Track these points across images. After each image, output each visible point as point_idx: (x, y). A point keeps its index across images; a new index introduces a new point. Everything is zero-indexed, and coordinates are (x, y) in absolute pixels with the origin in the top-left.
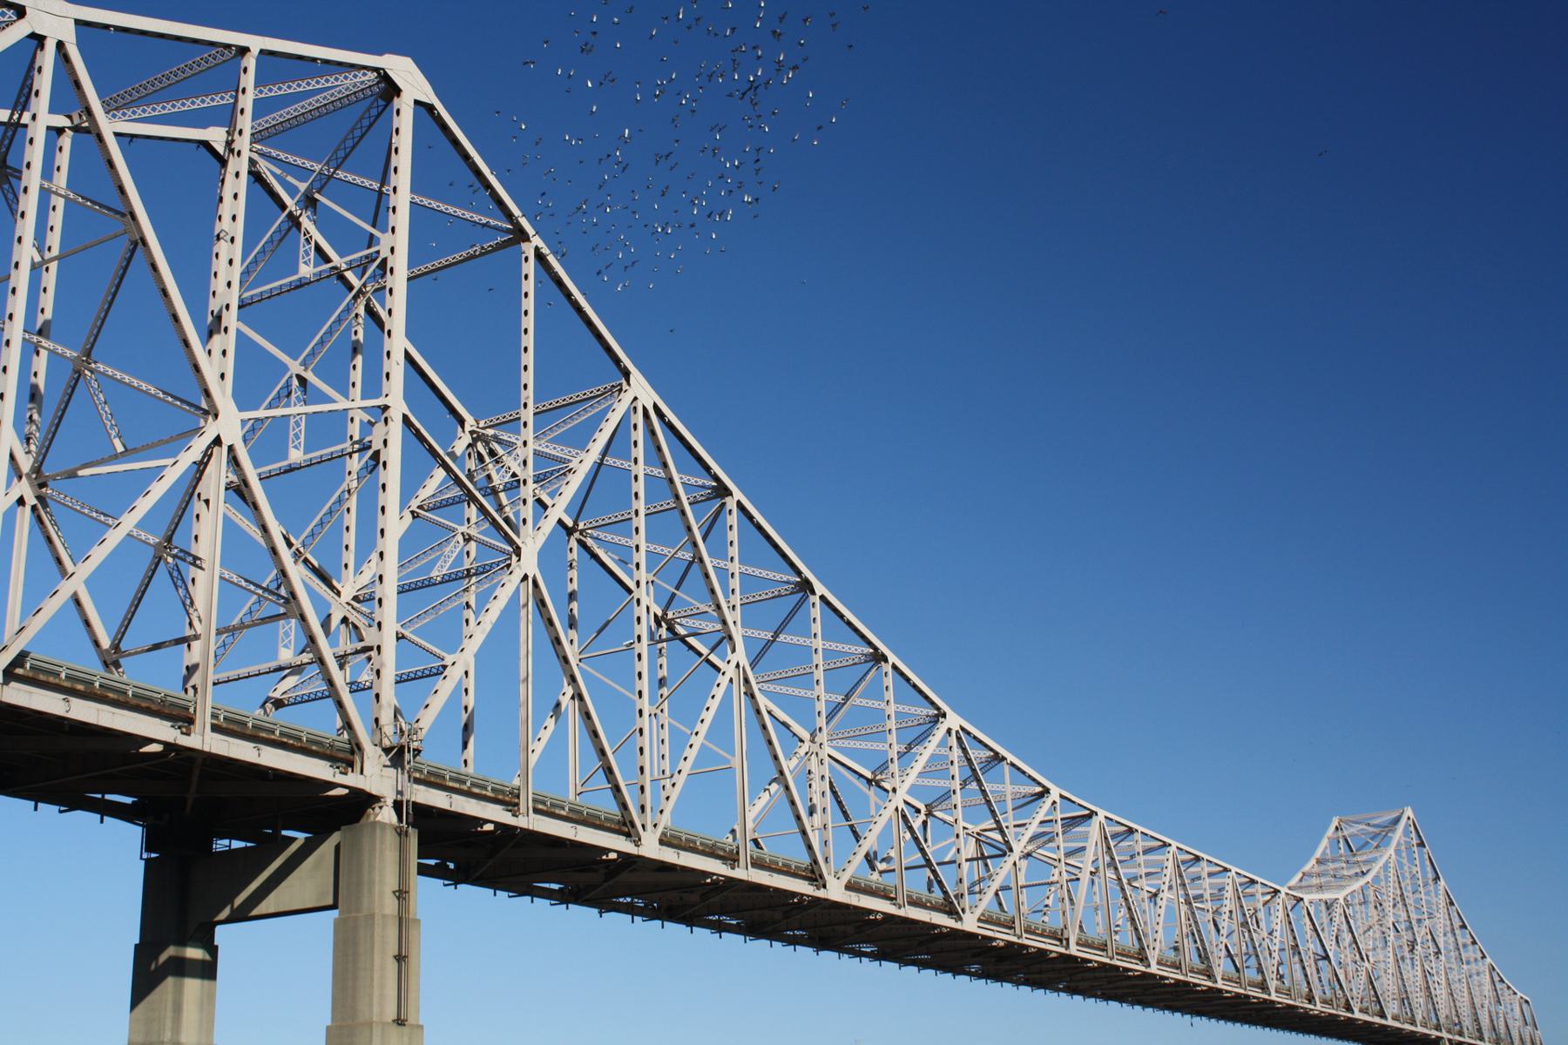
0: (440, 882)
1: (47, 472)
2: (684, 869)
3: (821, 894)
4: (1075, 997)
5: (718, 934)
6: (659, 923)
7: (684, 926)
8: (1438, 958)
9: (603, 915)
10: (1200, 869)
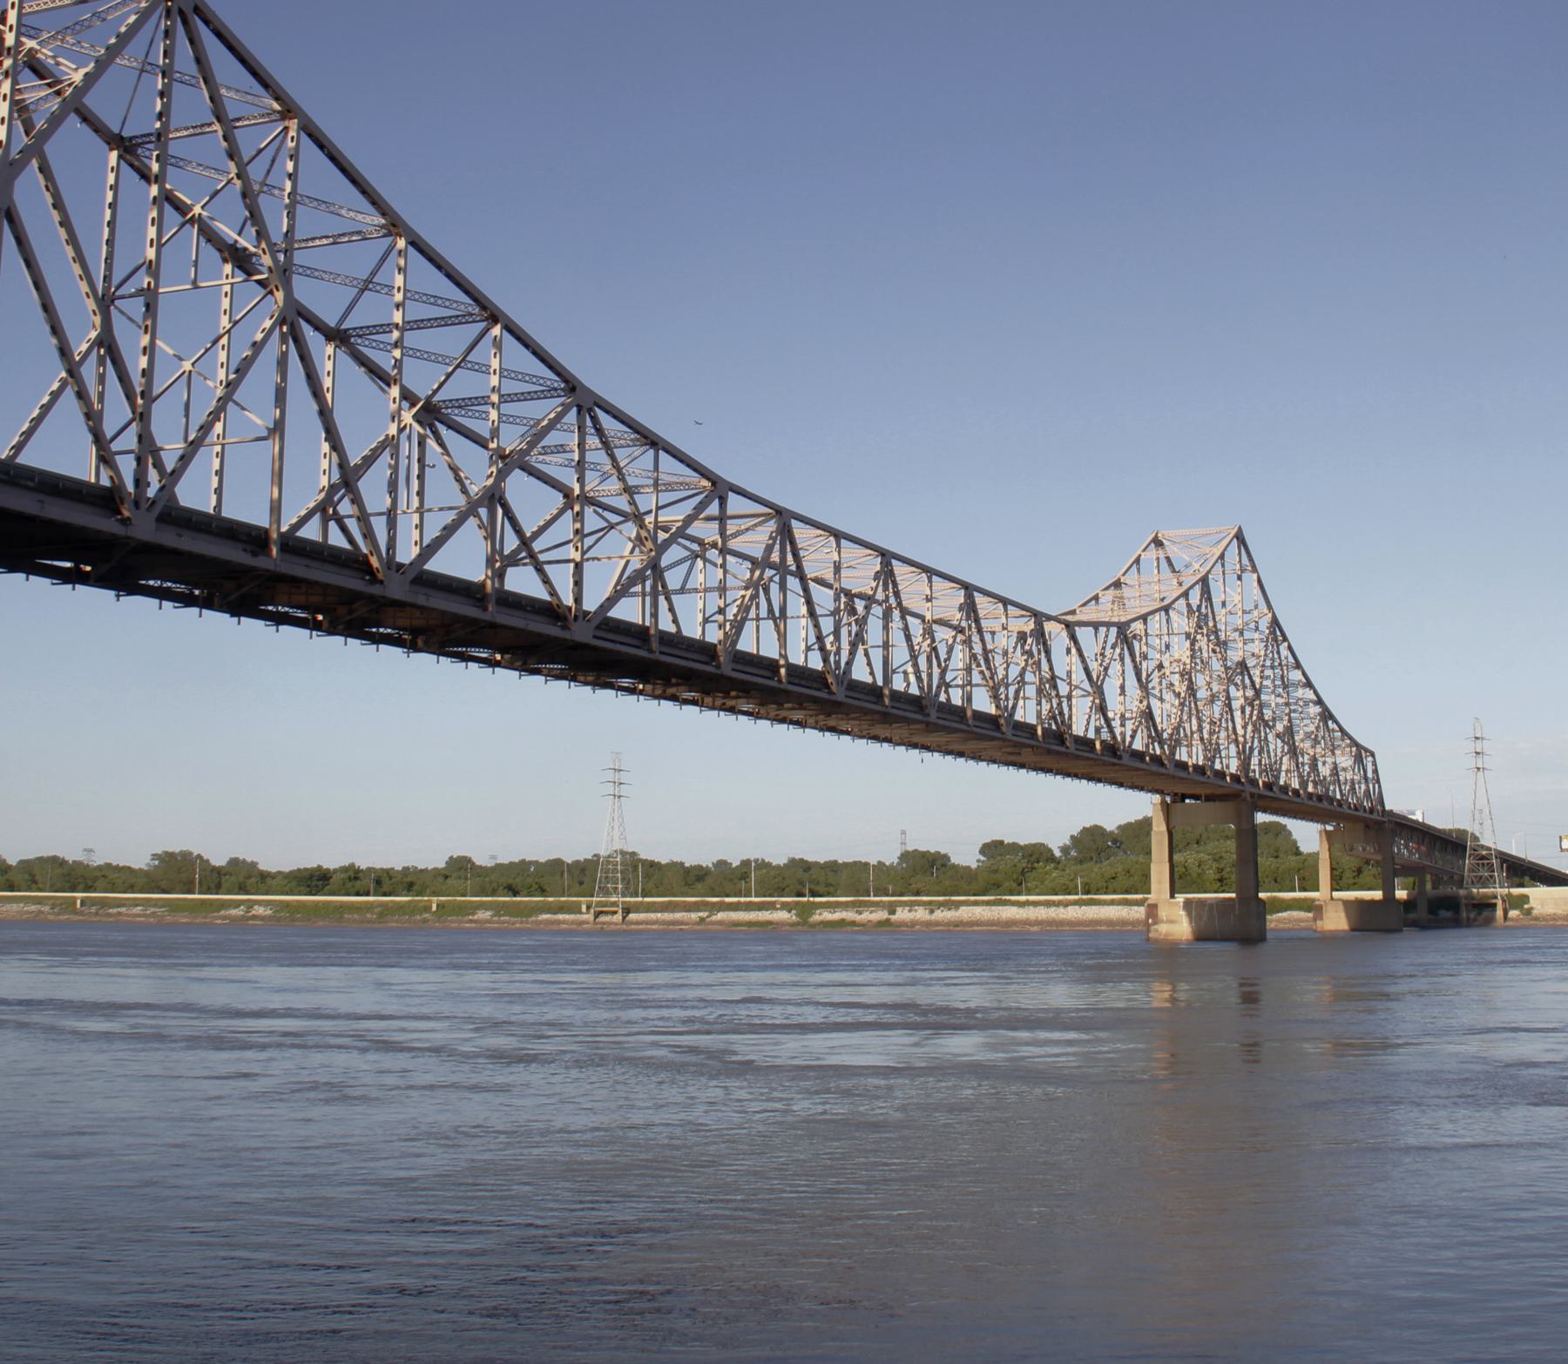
0: (263, 622)
1: (745, 575)
2: (51, 523)
3: (566, 635)
4: (980, 763)
5: (275, 628)
6: (70, 586)
7: (228, 615)
8: (30, 874)
9: (121, 598)
10: (1139, 913)
